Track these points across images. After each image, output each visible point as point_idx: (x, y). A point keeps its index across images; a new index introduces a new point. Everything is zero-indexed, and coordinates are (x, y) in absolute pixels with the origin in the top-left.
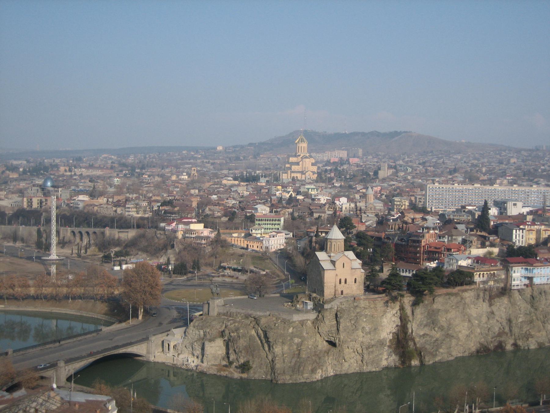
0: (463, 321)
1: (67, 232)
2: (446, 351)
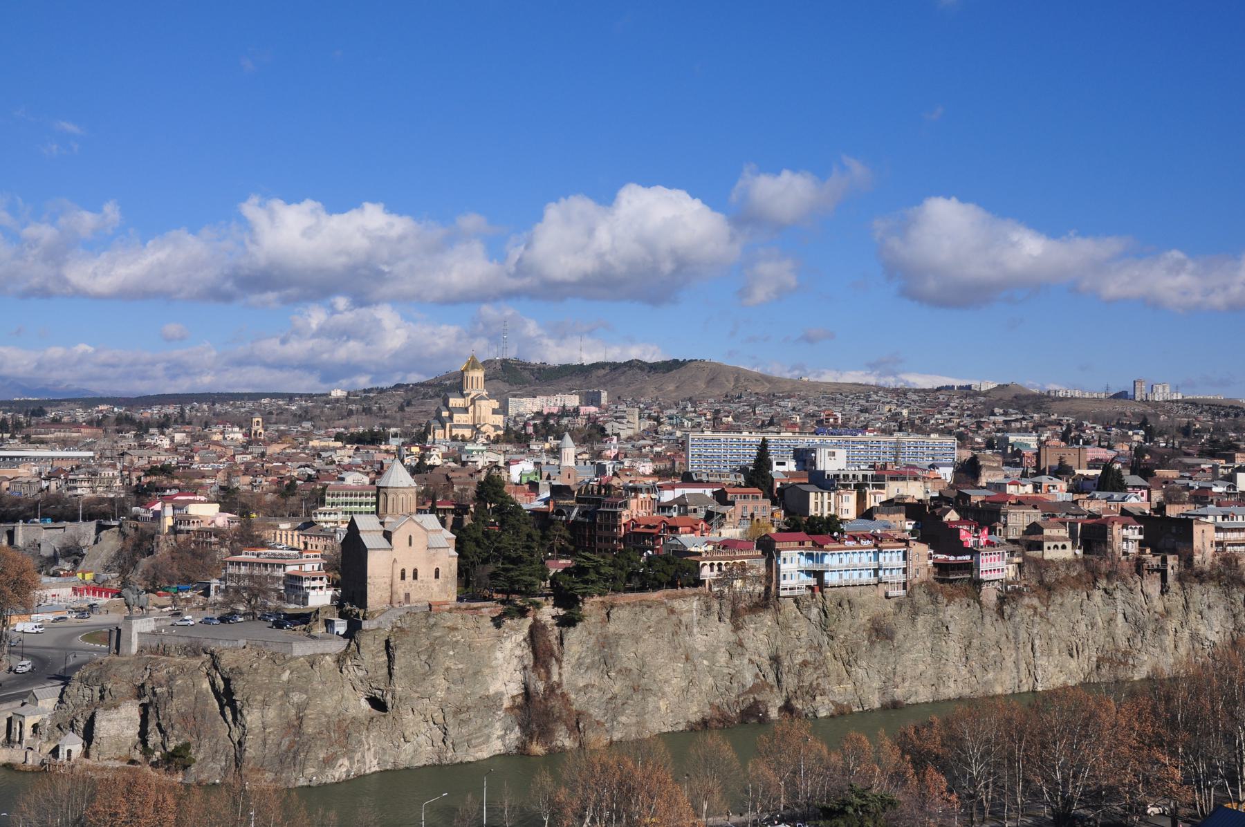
0: (674, 659)
2: (634, 720)
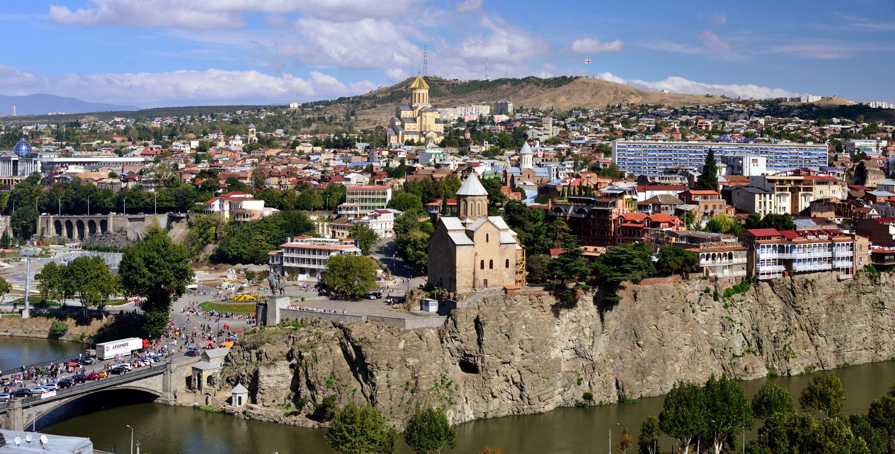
1: (19, 174)
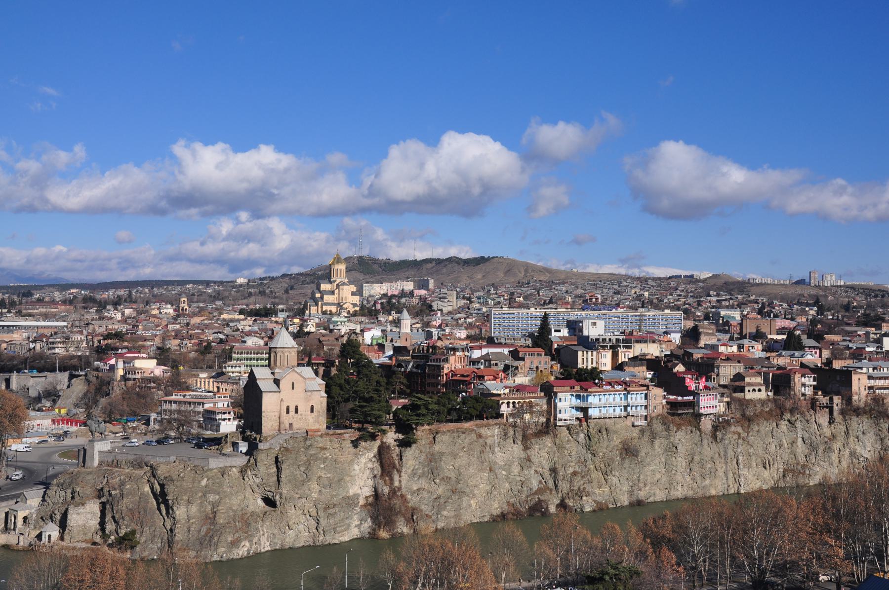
0: (481, 470)
2: (453, 513)
